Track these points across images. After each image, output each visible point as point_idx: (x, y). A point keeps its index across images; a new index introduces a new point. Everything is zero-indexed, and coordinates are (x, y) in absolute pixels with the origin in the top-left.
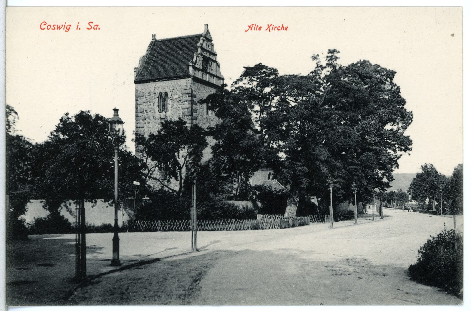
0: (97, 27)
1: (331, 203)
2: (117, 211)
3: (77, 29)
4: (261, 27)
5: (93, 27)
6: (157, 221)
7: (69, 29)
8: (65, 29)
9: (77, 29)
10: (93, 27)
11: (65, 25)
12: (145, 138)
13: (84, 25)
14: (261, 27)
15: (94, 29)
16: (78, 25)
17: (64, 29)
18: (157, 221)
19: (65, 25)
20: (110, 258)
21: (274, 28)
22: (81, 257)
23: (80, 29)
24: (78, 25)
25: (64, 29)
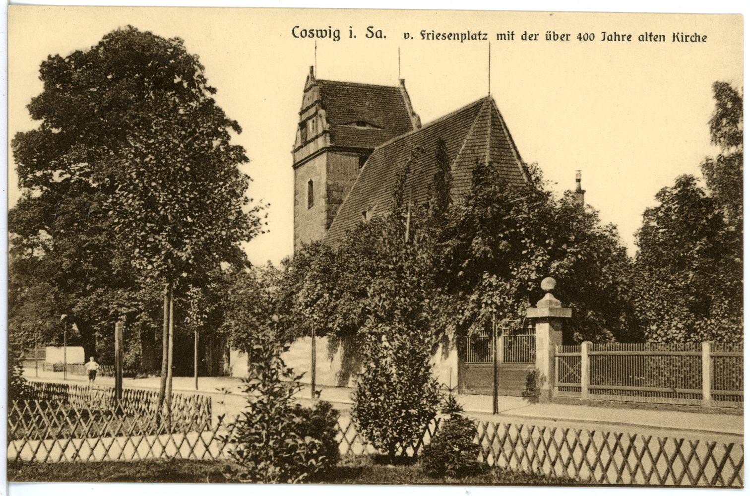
0: (380, 35)
1: (196, 370)
2: (342, 470)
3: (351, 37)
4: (630, 36)
5: (374, 34)
6: (677, 203)
7: (339, 36)
8: (333, 37)
9: (351, 37)
10: (374, 34)
11: (330, 31)
12: (458, 245)
13: (360, 31)
14: (630, 36)
15: (377, 37)
16: (351, 31)
17: (330, 37)
18: (677, 203)
19: (330, 31)
20: (28, 363)
22: (150, 65)
23: (355, 37)
24: (351, 31)
25: (330, 37)
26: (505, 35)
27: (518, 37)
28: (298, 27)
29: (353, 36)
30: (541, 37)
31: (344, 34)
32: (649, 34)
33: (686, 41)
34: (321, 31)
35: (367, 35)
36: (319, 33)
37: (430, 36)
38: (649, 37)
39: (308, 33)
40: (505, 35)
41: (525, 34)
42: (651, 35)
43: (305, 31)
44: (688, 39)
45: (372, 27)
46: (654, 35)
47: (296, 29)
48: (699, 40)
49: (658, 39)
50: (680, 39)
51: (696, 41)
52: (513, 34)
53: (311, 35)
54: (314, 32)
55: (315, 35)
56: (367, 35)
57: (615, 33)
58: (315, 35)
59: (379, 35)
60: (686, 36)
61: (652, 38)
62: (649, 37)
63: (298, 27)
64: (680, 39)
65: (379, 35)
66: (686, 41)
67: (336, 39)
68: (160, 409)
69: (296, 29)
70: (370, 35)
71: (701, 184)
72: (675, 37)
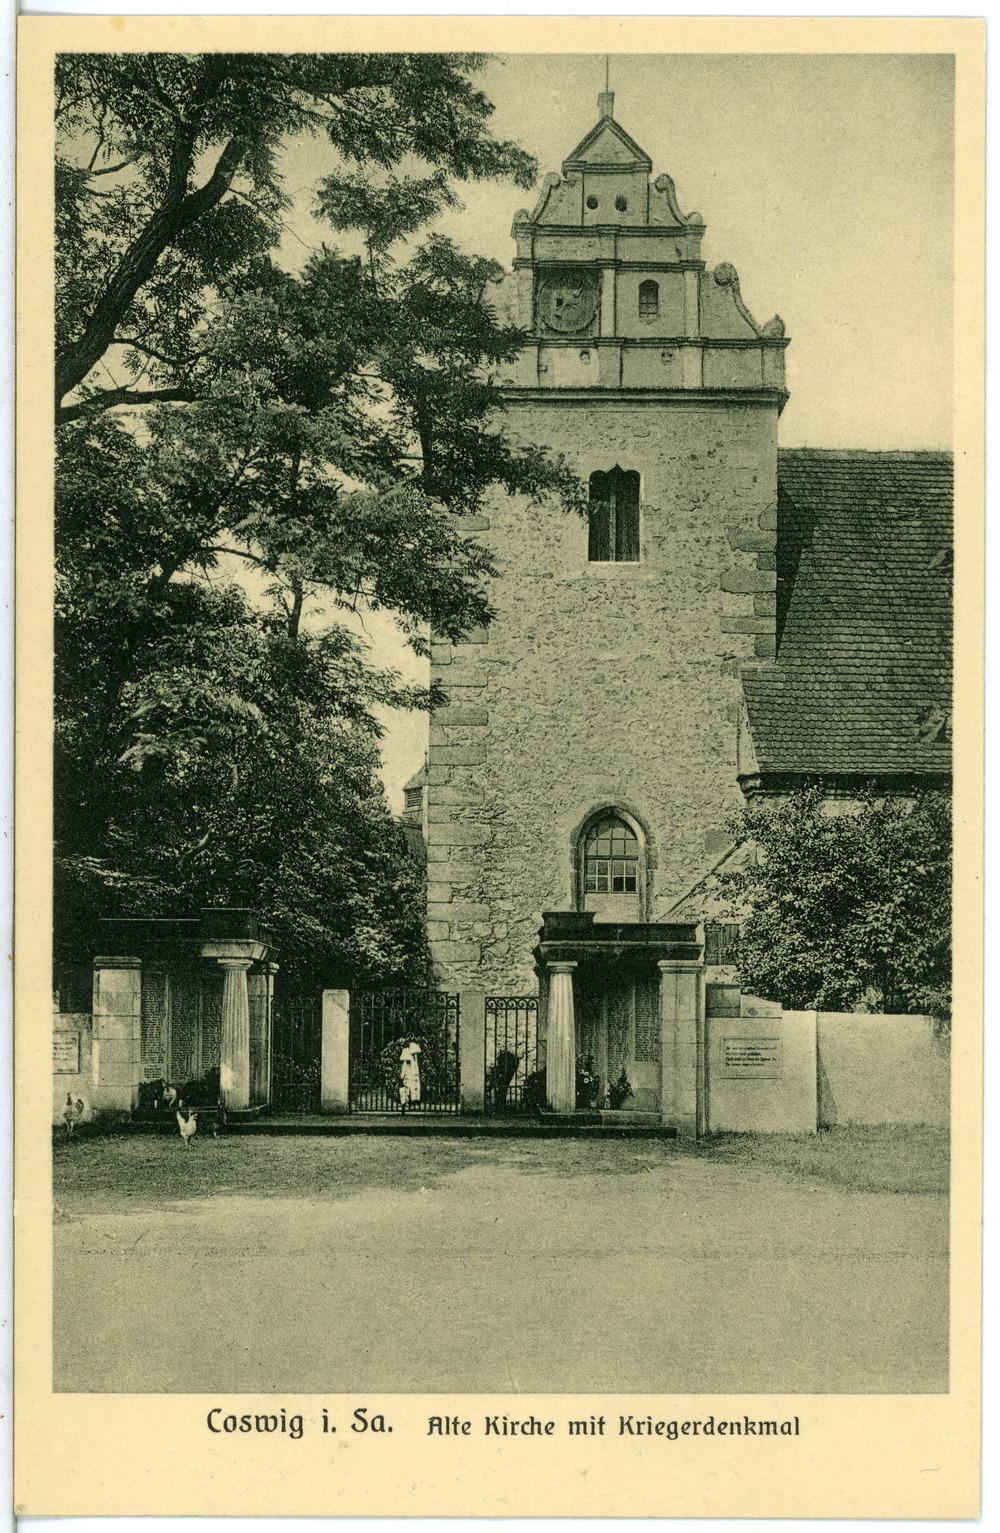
3: (326, 1430)
7: (301, 1429)
9: (326, 1430)
11: (283, 1417)
16: (325, 1418)
17: (284, 1430)
19: (283, 1417)
21: (509, 1427)
23: (334, 1430)
24: (325, 1418)
25: (284, 1430)
26: (585, 1424)
27: (611, 1426)
28: (219, 1411)
29: (330, 1428)
30: (561, 1428)
31: (313, 1426)
32: (452, 1420)
33: (513, 1433)
34: (265, 1417)
35: (353, 1427)
36: (262, 1422)
37: (644, 1429)
38: (452, 1427)
39: (239, 1423)
40: (585, 1424)
41: (712, 1423)
42: (456, 1423)
43: (234, 1418)
44: (518, 1429)
45: (364, 1410)
46: (461, 1421)
47: (214, 1415)
48: (539, 1432)
49: (727, 1430)
50: (501, 1428)
51: (532, 1433)
52: (601, 1423)
53: (245, 1427)
54: (252, 1421)
55: (369, 1426)
56: (353, 1427)
57: (746, 1418)
58: (369, 1426)
59: (377, 1426)
60: (513, 1424)
61: (459, 1427)
62: (452, 1427)
63: (219, 1411)
64: (501, 1428)
65: (377, 1426)
66: (639, 1433)
67: (673, 1436)
68: (197, 1068)
69: (214, 1415)
70: (360, 1425)
71: (470, 172)
72: (490, 1425)
